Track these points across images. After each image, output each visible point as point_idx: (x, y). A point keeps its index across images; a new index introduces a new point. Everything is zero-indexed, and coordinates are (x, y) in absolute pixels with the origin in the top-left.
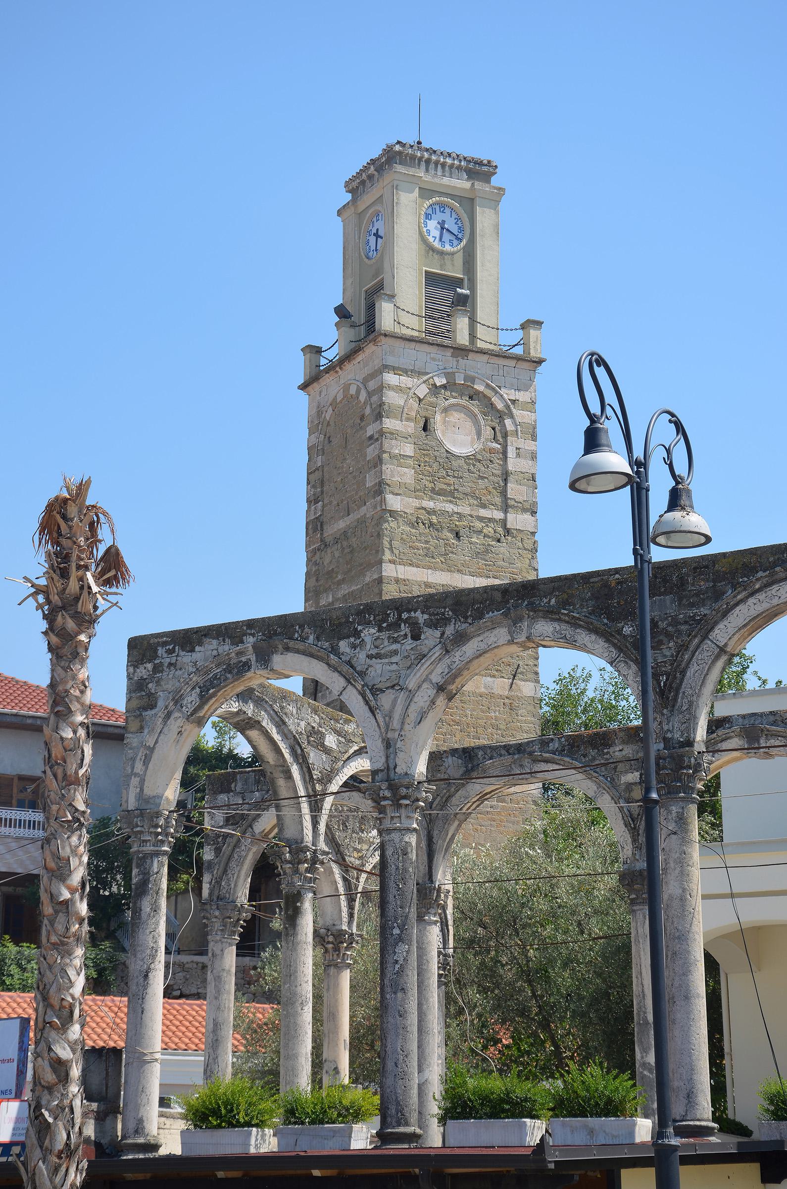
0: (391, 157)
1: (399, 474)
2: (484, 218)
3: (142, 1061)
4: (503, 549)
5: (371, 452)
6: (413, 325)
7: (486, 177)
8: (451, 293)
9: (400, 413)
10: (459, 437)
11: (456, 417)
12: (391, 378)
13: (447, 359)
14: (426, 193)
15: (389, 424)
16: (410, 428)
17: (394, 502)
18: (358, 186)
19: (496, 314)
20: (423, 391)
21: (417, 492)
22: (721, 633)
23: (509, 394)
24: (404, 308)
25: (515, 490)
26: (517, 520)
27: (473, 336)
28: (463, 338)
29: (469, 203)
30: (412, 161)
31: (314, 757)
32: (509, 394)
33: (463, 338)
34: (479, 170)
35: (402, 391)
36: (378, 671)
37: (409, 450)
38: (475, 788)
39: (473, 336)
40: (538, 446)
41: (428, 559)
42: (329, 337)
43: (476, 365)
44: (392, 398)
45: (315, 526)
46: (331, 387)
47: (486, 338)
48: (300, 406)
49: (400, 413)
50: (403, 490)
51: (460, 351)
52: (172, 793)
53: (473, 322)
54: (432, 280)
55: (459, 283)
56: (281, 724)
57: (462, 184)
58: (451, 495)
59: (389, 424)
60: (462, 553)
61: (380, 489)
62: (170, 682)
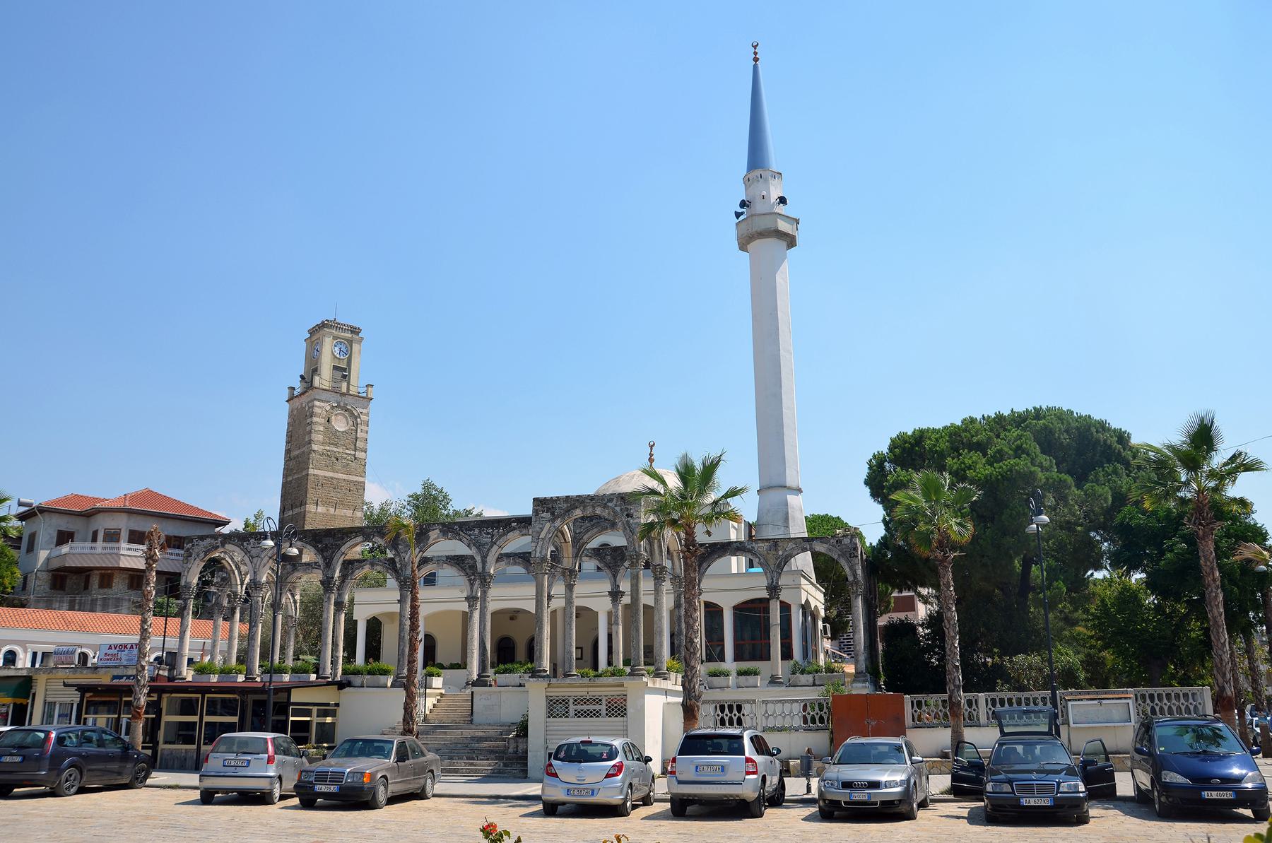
0: (323, 325)
1: (317, 437)
2: (355, 347)
3: (182, 656)
4: (353, 464)
5: (308, 428)
6: (326, 385)
7: (357, 334)
8: (342, 372)
9: (319, 416)
10: (340, 425)
11: (339, 417)
12: (317, 403)
13: (338, 397)
14: (335, 338)
15: (315, 419)
16: (323, 421)
17: (315, 447)
18: (313, 332)
19: (358, 381)
20: (328, 408)
21: (323, 443)
22: (343, 549)
23: (359, 410)
24: (325, 378)
25: (359, 444)
26: (359, 455)
27: (348, 389)
28: (344, 390)
29: (350, 342)
30: (331, 327)
31: (242, 568)
32: (359, 410)
33: (344, 390)
34: (355, 331)
35: (321, 408)
36: (254, 552)
37: (321, 429)
38: (296, 574)
39: (348, 389)
40: (370, 429)
41: (326, 468)
42: (297, 384)
43: (348, 399)
44: (317, 410)
45: (288, 452)
46: (297, 402)
47: (353, 390)
48: (286, 408)
49: (319, 416)
50: (318, 443)
51: (343, 394)
52: (195, 581)
53: (349, 384)
54: (335, 368)
55: (344, 370)
56: (232, 559)
57: (349, 335)
58: (336, 445)
59: (315, 419)
60: (339, 466)
61: (310, 442)
62: (196, 549)
